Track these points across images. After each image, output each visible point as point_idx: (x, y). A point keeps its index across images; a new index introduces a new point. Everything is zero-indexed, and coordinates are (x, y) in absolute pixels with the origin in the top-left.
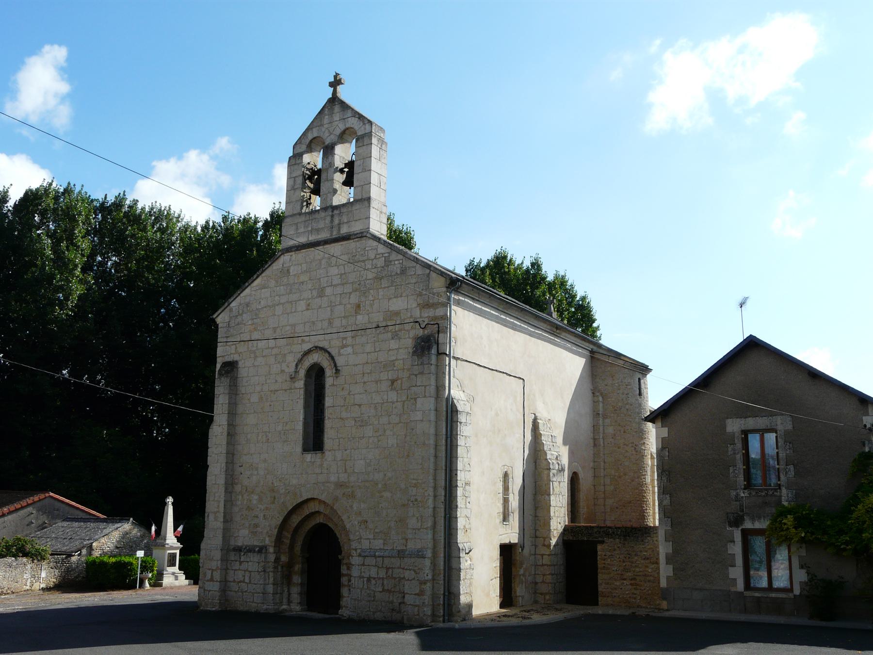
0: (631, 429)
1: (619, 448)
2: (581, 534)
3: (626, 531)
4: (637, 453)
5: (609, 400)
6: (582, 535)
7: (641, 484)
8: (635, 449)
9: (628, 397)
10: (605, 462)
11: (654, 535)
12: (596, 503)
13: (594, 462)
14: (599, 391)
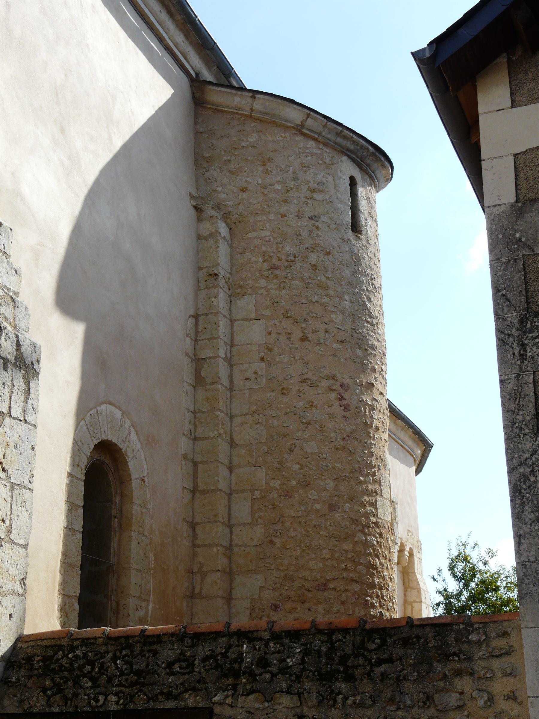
0: (326, 331)
1: (284, 392)
2: (94, 680)
3: (332, 649)
4: (347, 414)
5: (250, 235)
6: (95, 685)
7: (364, 521)
8: (341, 398)
9: (317, 228)
10: (232, 444)
11: (495, 664)
12: (197, 591)
13: (195, 439)
14: (218, 207)
